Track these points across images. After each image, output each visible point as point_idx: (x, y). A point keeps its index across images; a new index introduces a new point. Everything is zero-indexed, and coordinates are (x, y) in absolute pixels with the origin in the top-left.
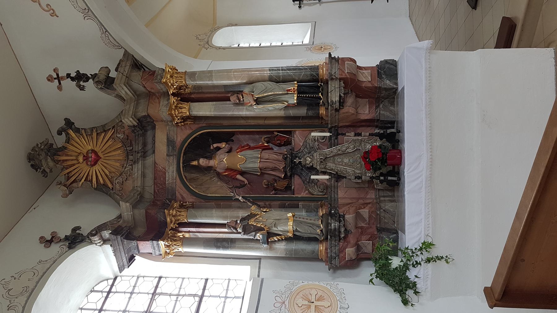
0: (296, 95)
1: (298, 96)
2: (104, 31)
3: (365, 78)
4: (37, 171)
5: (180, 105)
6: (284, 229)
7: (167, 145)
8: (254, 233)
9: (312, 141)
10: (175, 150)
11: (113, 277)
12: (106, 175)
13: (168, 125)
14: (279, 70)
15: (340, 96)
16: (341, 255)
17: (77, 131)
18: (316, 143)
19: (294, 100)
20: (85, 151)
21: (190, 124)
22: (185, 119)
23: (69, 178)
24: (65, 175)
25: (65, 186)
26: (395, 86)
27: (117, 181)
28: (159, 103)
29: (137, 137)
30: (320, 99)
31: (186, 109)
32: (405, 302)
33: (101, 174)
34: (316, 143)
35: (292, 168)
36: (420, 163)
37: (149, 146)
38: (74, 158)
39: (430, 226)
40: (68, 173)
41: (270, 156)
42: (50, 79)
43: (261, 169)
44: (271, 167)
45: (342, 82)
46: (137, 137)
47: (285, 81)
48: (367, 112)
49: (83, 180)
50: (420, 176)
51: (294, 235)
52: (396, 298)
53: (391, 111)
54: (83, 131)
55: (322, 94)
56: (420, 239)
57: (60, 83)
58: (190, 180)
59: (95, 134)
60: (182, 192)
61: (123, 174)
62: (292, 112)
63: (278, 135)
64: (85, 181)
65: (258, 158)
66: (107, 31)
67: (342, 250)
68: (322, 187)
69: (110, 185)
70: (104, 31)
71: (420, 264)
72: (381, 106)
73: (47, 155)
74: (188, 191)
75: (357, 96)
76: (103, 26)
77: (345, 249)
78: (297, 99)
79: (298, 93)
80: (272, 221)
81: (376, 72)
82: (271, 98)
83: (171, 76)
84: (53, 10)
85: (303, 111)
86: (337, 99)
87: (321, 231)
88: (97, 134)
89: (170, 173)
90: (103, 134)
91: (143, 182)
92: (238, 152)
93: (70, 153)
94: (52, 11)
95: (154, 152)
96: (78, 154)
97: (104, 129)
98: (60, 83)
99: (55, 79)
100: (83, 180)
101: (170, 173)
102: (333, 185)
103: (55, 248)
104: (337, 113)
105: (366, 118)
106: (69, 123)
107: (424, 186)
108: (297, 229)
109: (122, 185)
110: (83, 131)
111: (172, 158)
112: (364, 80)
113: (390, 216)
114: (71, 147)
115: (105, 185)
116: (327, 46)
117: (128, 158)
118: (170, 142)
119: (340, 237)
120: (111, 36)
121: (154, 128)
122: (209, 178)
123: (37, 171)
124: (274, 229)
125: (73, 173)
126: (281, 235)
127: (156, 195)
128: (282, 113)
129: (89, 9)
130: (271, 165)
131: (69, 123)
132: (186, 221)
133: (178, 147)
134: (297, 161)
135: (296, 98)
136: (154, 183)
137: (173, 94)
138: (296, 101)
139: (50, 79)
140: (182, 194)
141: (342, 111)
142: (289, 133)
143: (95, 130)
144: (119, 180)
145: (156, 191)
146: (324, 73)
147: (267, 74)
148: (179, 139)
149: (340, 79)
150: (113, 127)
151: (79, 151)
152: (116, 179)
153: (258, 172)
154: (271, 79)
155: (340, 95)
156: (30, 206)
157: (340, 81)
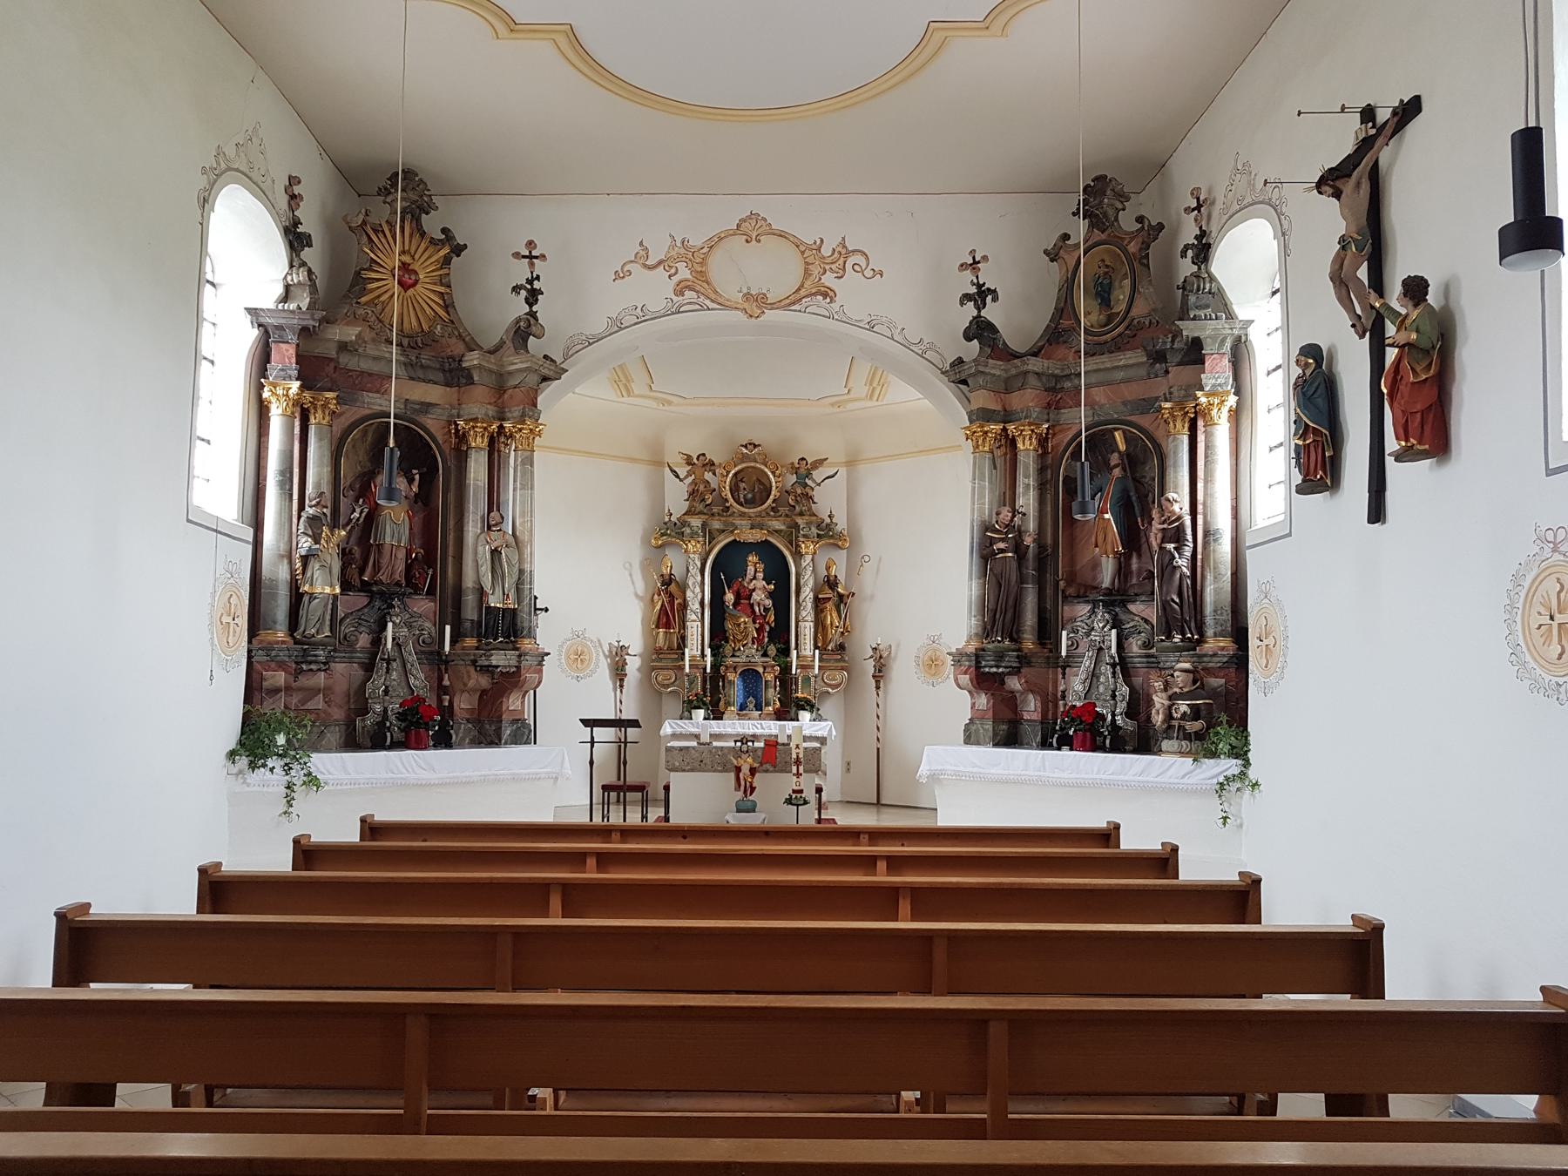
0: (501, 606)
1: (499, 608)
2: (591, 341)
3: (513, 702)
4: (388, 179)
5: (486, 434)
6: (317, 579)
7: (422, 402)
8: (310, 533)
9: (420, 625)
10: (413, 414)
11: (215, 282)
12: (379, 296)
13: (453, 407)
14: (531, 585)
15: (497, 667)
16: (273, 665)
17: (447, 261)
18: (418, 632)
19: (494, 601)
20: (415, 266)
21: (451, 442)
22: (462, 438)
23: (376, 231)
24: (380, 225)
25: (364, 223)
26: (503, 741)
27: (369, 312)
28: (490, 404)
29: (441, 360)
30: (495, 640)
31: (478, 442)
32: (232, 755)
33: (380, 287)
34: (418, 632)
35: (382, 594)
36: (424, 769)
37: (420, 374)
38: (407, 248)
39: (339, 787)
40: (383, 232)
41: (399, 561)
42: (531, 244)
43: (378, 545)
44: (381, 561)
45: (514, 669)
46: (441, 360)
47: (518, 590)
48: (463, 706)
49: (372, 255)
50: (408, 771)
51: (302, 595)
52: (232, 744)
53: (463, 739)
54: (446, 271)
55: (501, 642)
56: (321, 773)
57: (524, 257)
58: (365, 432)
59: (442, 289)
60: (348, 415)
61: (381, 324)
62: (470, 600)
63: (428, 574)
64: (372, 258)
65: (399, 542)
66: (590, 344)
67: (281, 666)
68: (353, 638)
69: (363, 300)
70: (591, 341)
71: (287, 774)
72: (470, 726)
73: (414, 202)
74: (349, 426)
75: (484, 692)
76: (597, 341)
77: (284, 670)
78: (495, 607)
79: (504, 610)
80: (329, 562)
81: (517, 718)
82: (499, 571)
83: (531, 430)
84: (623, 277)
85: (470, 612)
86: (494, 663)
87: (313, 636)
88: (442, 293)
89: (379, 401)
90: (441, 302)
91: (367, 356)
92: (408, 511)
93: (414, 242)
94: (622, 275)
95: (412, 379)
96: (413, 253)
97: (448, 306)
98: (524, 257)
99: (530, 252)
100: (372, 255)
101: (379, 401)
102: (354, 655)
103: (282, 201)
104: (469, 662)
105: (455, 704)
106: (459, 250)
107: (394, 776)
108: (317, 600)
109: (364, 320)
110: (446, 271)
111: (402, 407)
112: (510, 701)
113: (313, 740)
114: (423, 246)
115: (364, 292)
116: (237, 635)
117: (404, 336)
118: (426, 407)
119: (302, 663)
120: (583, 348)
121: (448, 385)
122: (361, 459)
123: (388, 179)
124: (317, 566)
125: (383, 240)
126: (303, 574)
127: (343, 371)
128: (469, 582)
129: (621, 329)
130: (385, 561)
131: (459, 250)
132: (312, 420)
133: (417, 418)
134: (396, 602)
135: (498, 605)
136: (363, 372)
137: (501, 427)
138: (492, 605)
139: (531, 244)
140: (345, 415)
141: (472, 669)
142: (431, 592)
143: (448, 291)
144: (370, 315)
145: (350, 374)
146: (526, 644)
147: (527, 567)
148: (429, 421)
149: (518, 668)
150: (452, 322)
151: (417, 257)
152: (373, 311)
153: (375, 541)
154: (521, 572)
155: (499, 666)
156: (324, 149)
157: (516, 667)
